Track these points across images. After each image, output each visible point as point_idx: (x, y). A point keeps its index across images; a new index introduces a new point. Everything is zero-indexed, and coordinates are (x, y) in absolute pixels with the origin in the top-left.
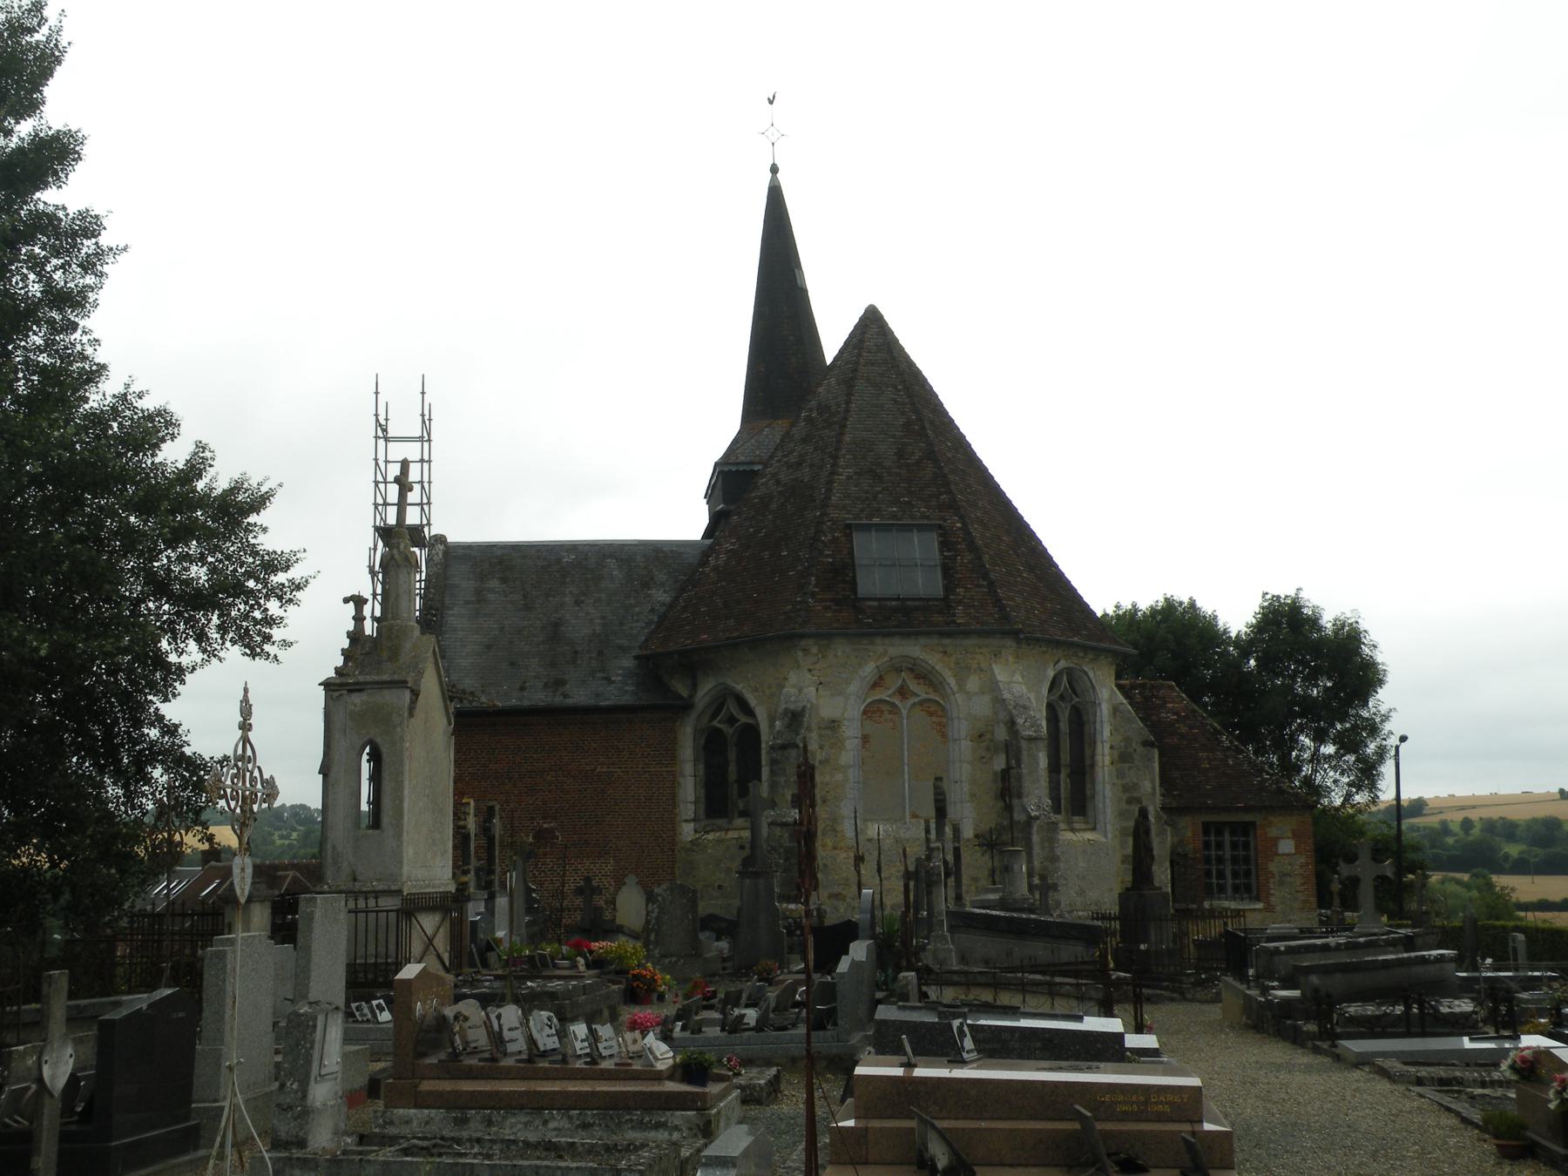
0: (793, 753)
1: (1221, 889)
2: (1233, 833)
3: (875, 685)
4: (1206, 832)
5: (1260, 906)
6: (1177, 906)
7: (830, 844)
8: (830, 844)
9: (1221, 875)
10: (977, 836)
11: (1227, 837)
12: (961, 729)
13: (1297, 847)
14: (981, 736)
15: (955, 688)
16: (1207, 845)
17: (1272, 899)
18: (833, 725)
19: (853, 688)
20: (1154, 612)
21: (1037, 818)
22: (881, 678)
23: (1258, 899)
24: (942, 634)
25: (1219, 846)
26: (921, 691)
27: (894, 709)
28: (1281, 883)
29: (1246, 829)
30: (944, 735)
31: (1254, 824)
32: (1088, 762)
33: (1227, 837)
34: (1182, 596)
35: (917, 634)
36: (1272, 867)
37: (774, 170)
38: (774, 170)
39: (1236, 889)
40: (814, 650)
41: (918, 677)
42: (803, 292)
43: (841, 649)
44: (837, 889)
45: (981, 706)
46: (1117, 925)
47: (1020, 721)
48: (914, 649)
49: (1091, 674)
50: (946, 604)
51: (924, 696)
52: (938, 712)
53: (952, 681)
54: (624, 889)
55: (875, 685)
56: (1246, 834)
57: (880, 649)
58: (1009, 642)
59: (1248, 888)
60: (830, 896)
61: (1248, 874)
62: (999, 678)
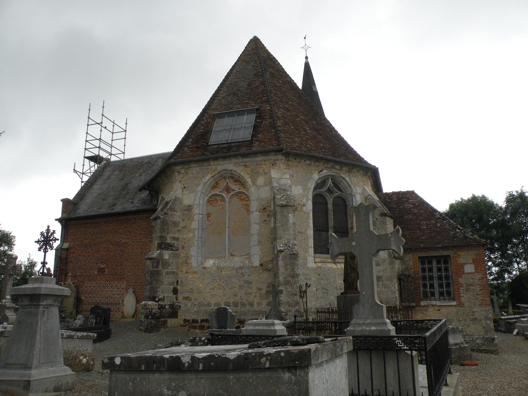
0: (159, 221)
1: (433, 294)
2: (439, 262)
3: (214, 187)
4: (423, 263)
5: (455, 303)
6: (404, 304)
7: (184, 270)
8: (184, 270)
9: (432, 286)
10: (261, 265)
11: (434, 264)
12: (254, 206)
13: (476, 269)
14: (264, 209)
15: (251, 184)
16: (423, 270)
17: (462, 299)
18: (189, 208)
19: (200, 188)
20: (469, 200)
21: (281, 251)
22: (217, 183)
23: (454, 299)
24: (244, 156)
25: (431, 270)
26: (236, 188)
27: (223, 199)
28: (467, 290)
29: (446, 259)
30: (248, 211)
31: (449, 256)
32: (349, 226)
33: (434, 264)
34: (479, 194)
35: (230, 157)
36: (461, 281)
37: (307, 58)
38: (307, 58)
39: (441, 294)
40: (183, 171)
41: (236, 181)
42: (316, 94)
43: (195, 169)
44: (187, 295)
45: (265, 193)
46: (336, 317)
47: (278, 197)
48: (229, 165)
49: (348, 179)
50: (249, 143)
51: (237, 190)
52: (243, 197)
53: (249, 180)
54: (128, 295)
55: (214, 187)
56: (446, 262)
57: (214, 167)
58: (280, 157)
59: (449, 294)
60: (184, 298)
61: (448, 285)
62: (273, 176)
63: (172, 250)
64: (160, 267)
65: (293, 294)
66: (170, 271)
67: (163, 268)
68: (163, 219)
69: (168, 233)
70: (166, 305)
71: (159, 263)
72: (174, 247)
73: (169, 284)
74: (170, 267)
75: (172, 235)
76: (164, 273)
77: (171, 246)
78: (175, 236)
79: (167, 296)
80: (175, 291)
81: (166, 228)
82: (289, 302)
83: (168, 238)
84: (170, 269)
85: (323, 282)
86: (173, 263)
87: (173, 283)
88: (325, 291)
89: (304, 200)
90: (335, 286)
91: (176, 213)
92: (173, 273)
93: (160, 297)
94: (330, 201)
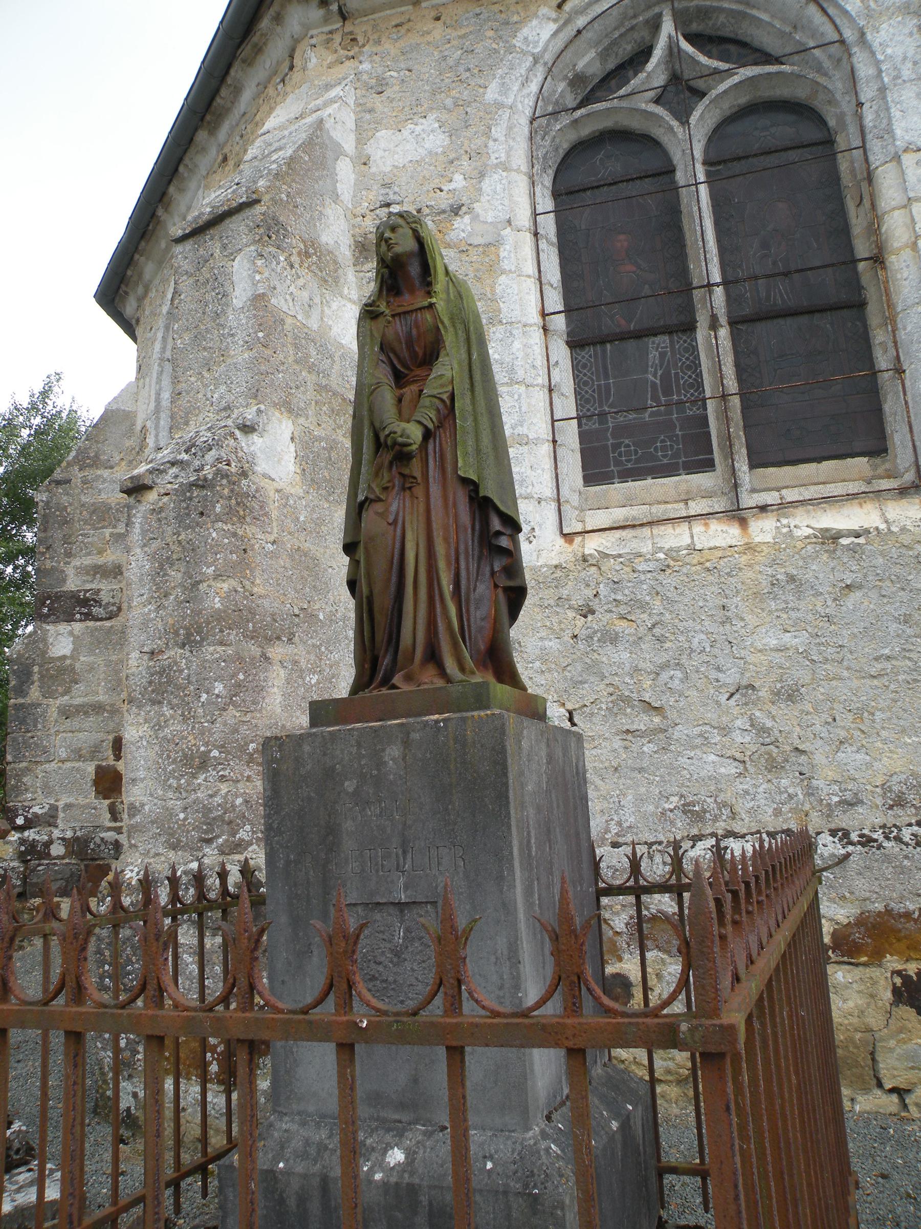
63: (88, 616)
64: (35, 693)
65: (187, 760)
66: (78, 701)
67: (48, 694)
68: (47, 503)
69: (69, 554)
70: (50, 842)
71: (29, 674)
72: (98, 602)
73: (78, 755)
74: (81, 687)
75: (88, 561)
76: (53, 713)
77: (85, 602)
78: (100, 560)
79: (68, 806)
80: (109, 783)
81: (59, 535)
82: (170, 814)
83: (70, 571)
84: (79, 696)
85: (621, 655)
86: (91, 668)
87: (95, 750)
88: (642, 722)
89: (459, 182)
90: (731, 677)
91: (106, 473)
92: (98, 708)
93: (36, 809)
94: (688, 143)
